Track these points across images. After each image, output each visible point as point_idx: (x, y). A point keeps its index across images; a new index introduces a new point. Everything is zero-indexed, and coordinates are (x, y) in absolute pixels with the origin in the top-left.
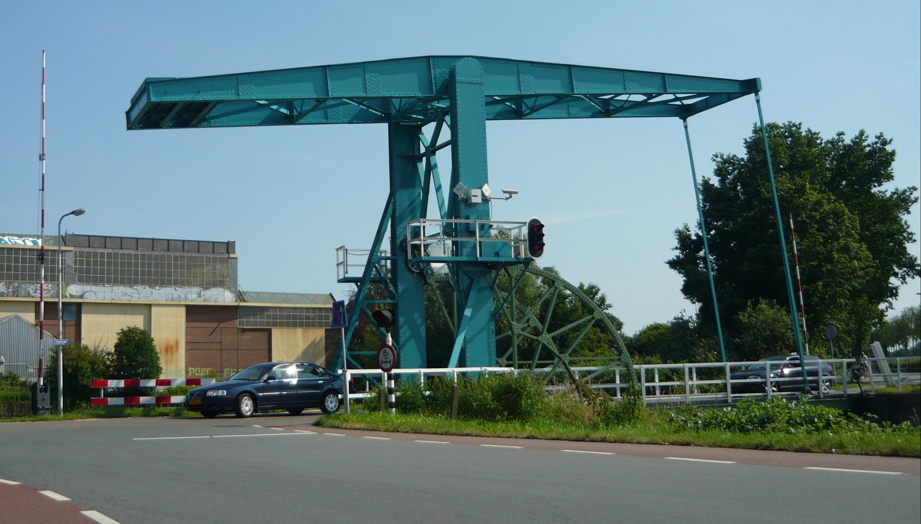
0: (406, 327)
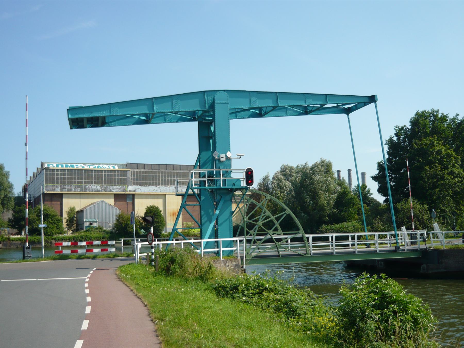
0: (205, 215)
